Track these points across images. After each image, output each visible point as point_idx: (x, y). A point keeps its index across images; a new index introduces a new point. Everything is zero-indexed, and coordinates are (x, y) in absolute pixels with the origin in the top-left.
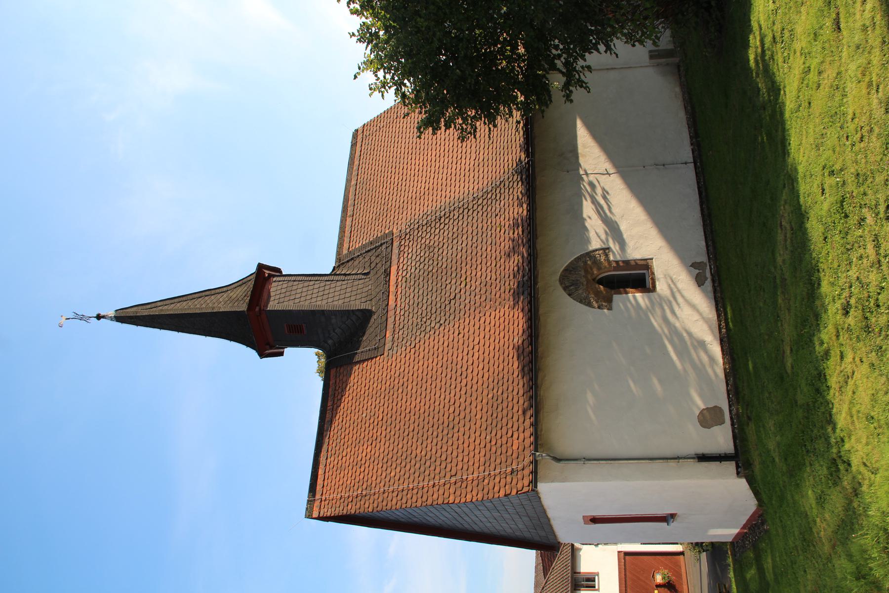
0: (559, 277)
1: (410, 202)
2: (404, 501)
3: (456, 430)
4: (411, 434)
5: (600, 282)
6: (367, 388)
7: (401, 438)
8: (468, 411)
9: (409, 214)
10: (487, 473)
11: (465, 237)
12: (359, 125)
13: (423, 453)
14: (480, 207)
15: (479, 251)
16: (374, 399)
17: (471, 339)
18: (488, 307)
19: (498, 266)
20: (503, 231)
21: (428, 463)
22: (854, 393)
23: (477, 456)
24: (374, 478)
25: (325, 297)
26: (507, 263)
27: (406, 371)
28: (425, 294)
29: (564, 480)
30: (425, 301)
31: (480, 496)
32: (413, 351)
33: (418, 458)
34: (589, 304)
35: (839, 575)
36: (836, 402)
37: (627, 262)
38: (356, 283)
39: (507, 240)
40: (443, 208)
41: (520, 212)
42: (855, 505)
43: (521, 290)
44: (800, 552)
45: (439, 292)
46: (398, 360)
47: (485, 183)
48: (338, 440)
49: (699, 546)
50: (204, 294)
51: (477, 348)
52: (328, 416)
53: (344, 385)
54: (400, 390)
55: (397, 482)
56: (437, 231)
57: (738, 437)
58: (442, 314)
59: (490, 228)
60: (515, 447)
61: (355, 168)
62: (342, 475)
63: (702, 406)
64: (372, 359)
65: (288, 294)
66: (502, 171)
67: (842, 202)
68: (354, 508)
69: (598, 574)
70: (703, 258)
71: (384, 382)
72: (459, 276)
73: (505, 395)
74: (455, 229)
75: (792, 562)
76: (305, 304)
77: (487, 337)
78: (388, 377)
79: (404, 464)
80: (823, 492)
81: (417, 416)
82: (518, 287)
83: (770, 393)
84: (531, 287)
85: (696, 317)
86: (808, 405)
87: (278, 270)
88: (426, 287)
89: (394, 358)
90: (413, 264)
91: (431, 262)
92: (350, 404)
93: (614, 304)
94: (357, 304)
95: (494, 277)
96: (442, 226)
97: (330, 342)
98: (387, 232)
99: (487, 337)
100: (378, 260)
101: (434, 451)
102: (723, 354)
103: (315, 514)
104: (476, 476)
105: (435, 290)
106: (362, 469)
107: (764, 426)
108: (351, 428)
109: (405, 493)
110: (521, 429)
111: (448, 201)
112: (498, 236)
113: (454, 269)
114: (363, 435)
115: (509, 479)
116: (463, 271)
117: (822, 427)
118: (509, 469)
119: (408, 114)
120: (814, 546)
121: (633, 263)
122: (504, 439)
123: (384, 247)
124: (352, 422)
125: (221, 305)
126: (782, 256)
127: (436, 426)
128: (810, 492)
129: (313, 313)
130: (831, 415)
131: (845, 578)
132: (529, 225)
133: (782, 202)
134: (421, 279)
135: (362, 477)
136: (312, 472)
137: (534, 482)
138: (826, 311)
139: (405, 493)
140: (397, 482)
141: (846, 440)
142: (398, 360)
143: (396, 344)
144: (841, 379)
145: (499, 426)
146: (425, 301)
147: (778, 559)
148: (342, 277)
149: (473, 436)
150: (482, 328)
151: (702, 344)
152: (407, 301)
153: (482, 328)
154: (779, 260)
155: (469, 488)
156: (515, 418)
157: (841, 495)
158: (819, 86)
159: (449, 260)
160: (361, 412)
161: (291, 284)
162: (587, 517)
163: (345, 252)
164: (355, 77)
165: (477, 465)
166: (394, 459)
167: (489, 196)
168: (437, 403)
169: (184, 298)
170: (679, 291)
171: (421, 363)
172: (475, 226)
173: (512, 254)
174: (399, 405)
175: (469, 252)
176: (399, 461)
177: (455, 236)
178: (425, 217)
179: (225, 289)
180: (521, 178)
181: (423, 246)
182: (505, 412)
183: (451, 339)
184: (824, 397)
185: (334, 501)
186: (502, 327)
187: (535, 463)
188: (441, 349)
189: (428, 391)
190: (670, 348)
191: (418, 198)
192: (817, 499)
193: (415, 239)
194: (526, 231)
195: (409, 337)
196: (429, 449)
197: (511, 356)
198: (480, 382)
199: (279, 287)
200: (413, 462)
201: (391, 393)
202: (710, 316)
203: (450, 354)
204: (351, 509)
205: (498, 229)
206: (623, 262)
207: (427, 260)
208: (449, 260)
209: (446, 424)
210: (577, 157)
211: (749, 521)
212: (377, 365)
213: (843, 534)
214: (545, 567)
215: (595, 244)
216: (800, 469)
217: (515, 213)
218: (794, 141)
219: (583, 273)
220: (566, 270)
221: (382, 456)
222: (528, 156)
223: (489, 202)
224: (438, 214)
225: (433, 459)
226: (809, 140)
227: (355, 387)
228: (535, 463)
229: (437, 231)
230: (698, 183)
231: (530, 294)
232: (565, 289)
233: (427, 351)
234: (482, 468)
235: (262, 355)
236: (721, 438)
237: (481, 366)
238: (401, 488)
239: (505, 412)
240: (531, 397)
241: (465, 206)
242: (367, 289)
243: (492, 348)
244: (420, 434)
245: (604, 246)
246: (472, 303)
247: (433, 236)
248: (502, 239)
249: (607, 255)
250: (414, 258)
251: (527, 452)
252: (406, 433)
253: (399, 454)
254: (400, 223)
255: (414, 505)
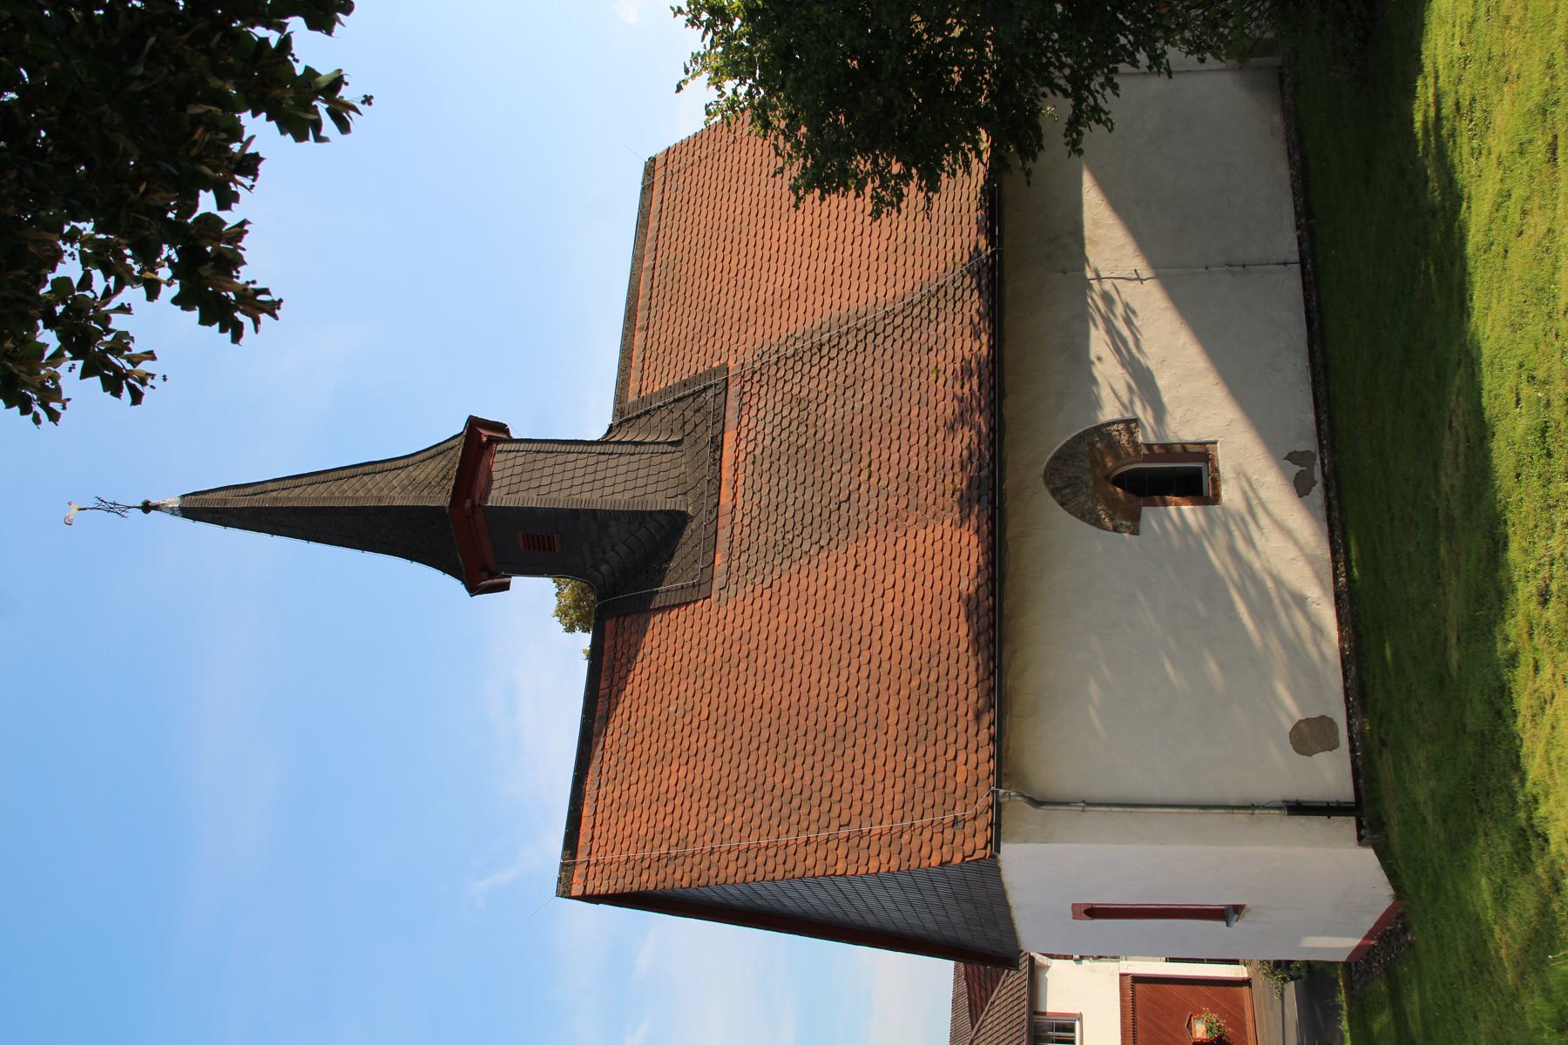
0: (1044, 473)
1: (760, 311)
2: (751, 868)
3: (849, 742)
4: (764, 748)
5: (1118, 481)
6: (677, 658)
7: (744, 754)
8: (872, 709)
9: (760, 332)
10: (907, 823)
11: (868, 386)
12: (657, 149)
13: (788, 782)
14: (898, 332)
15: (896, 414)
16: (691, 680)
17: (879, 578)
18: (911, 521)
19: (932, 445)
20: (941, 381)
21: (796, 802)
22: (1553, 728)
23: (889, 791)
24: (692, 826)
25: (598, 484)
26: (948, 442)
27: (755, 630)
28: (791, 488)
29: (1046, 840)
30: (790, 501)
31: (894, 864)
32: (767, 593)
33: (777, 792)
34: (1098, 523)
35: (1531, 1023)
36: (1526, 736)
37: (1167, 447)
38: (656, 460)
39: (950, 397)
40: (826, 327)
41: (975, 348)
42: (1555, 906)
43: (975, 494)
44: (1468, 983)
45: (818, 486)
46: (739, 609)
47: (909, 286)
48: (622, 754)
49: (1281, 968)
50: (360, 470)
51: (889, 594)
52: (601, 707)
53: (632, 652)
54: (743, 666)
55: (736, 834)
56: (815, 370)
57: (1359, 773)
58: (825, 528)
59: (916, 372)
60: (960, 778)
61: (651, 234)
62: (629, 817)
63: (1298, 716)
64: (688, 604)
65: (526, 476)
66: (942, 267)
67: (1544, 430)
68: (653, 878)
69: (1080, 1017)
70: (1309, 444)
71: (710, 649)
72: (856, 458)
73: (943, 684)
74: (850, 369)
75: (1453, 1000)
76: (562, 497)
77: (910, 575)
78: (720, 640)
79: (749, 801)
80: (1504, 881)
81: (775, 715)
82: (969, 487)
83: (1420, 704)
84: (993, 489)
85: (1292, 552)
86: (1482, 734)
87: (502, 428)
88: (792, 474)
89: (731, 606)
90: (768, 430)
91: (802, 429)
92: (643, 687)
93: (1143, 523)
94: (659, 501)
95: (923, 466)
96: (824, 361)
97: (604, 568)
98: (716, 364)
99: (910, 575)
100: (698, 418)
101: (807, 779)
102: (1340, 630)
103: (577, 890)
104: (891, 834)
105: (809, 481)
106: (669, 809)
107: (1408, 760)
108: (648, 732)
109: (752, 854)
110: (972, 746)
111: (836, 314)
112: (932, 390)
113: (847, 444)
114: (669, 746)
115: (948, 834)
116: (865, 451)
117: (1505, 775)
118: (949, 818)
119: (782, 170)
120: (1490, 973)
121: (1178, 449)
122: (940, 764)
123: (710, 393)
124: (648, 720)
125: (395, 492)
126: (1450, 479)
127: (811, 735)
128: (1483, 881)
129: (575, 513)
130: (1518, 757)
131: (1540, 1030)
132: (992, 374)
133: (1454, 389)
134: (784, 459)
135: (668, 822)
136: (570, 812)
137: (995, 842)
138: (1514, 590)
139: (752, 854)
140: (736, 834)
141: (1542, 799)
142: (739, 609)
143: (733, 579)
144: (1535, 703)
145: (931, 739)
146: (790, 501)
147: (1429, 995)
148: (631, 449)
149: (881, 755)
150: (900, 559)
151: (1300, 601)
152: (756, 500)
153: (900, 559)
154: (1445, 484)
155: (874, 850)
156: (961, 727)
157: (1533, 890)
158: (1521, 234)
159: (838, 428)
160: (665, 703)
161: (530, 457)
162: (1080, 905)
163: (632, 397)
164: (679, 88)
165: (888, 807)
166: (732, 791)
167: (916, 311)
168: (814, 693)
169: (322, 477)
170: (1262, 504)
171: (783, 617)
172: (888, 366)
173: (958, 426)
174: (741, 692)
175: (877, 414)
176: (740, 796)
177: (850, 382)
178: (791, 341)
179: (402, 463)
180: (979, 284)
181: (788, 397)
182: (942, 713)
183: (840, 575)
184: (1507, 727)
185: (614, 867)
186: (938, 559)
187: (997, 807)
188: (821, 594)
189: (797, 670)
190: (1241, 608)
191: (777, 304)
192: (1495, 893)
193: (772, 382)
194: (986, 386)
195: (760, 567)
196: (798, 775)
197: (954, 613)
198: (896, 658)
199: (510, 463)
200: (768, 797)
201: (726, 669)
202: (1319, 552)
203: (839, 603)
204: (648, 881)
205: (933, 377)
206: (1161, 446)
207: (795, 424)
208: (838, 428)
209: (830, 731)
210: (1082, 246)
211: (1378, 923)
212: (696, 617)
213: (1536, 954)
214: (973, 1004)
215: (1110, 411)
216: (1468, 841)
217: (966, 349)
218: (1478, 301)
219: (1087, 465)
220: (1056, 458)
221: (707, 786)
222: (991, 243)
223: (916, 324)
224: (816, 338)
225: (806, 794)
226: (1500, 311)
227: (654, 656)
228: (997, 807)
229: (815, 370)
230: (1307, 302)
231: (992, 503)
232: (1055, 492)
233: (794, 594)
234: (898, 814)
235: (474, 589)
236: (1330, 774)
237: (897, 629)
238: (744, 844)
239: (942, 713)
240: (991, 690)
241: (870, 328)
242: (677, 472)
243: (918, 596)
244: (781, 748)
245: (1128, 416)
246: (882, 510)
247: (806, 379)
248: (940, 396)
249: (1131, 433)
250: (769, 418)
251: (983, 789)
252: (755, 744)
253: (741, 783)
254: (741, 349)
255: (769, 877)
